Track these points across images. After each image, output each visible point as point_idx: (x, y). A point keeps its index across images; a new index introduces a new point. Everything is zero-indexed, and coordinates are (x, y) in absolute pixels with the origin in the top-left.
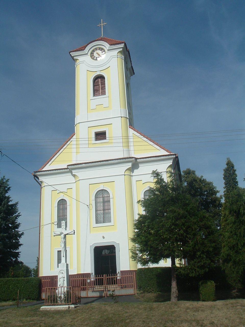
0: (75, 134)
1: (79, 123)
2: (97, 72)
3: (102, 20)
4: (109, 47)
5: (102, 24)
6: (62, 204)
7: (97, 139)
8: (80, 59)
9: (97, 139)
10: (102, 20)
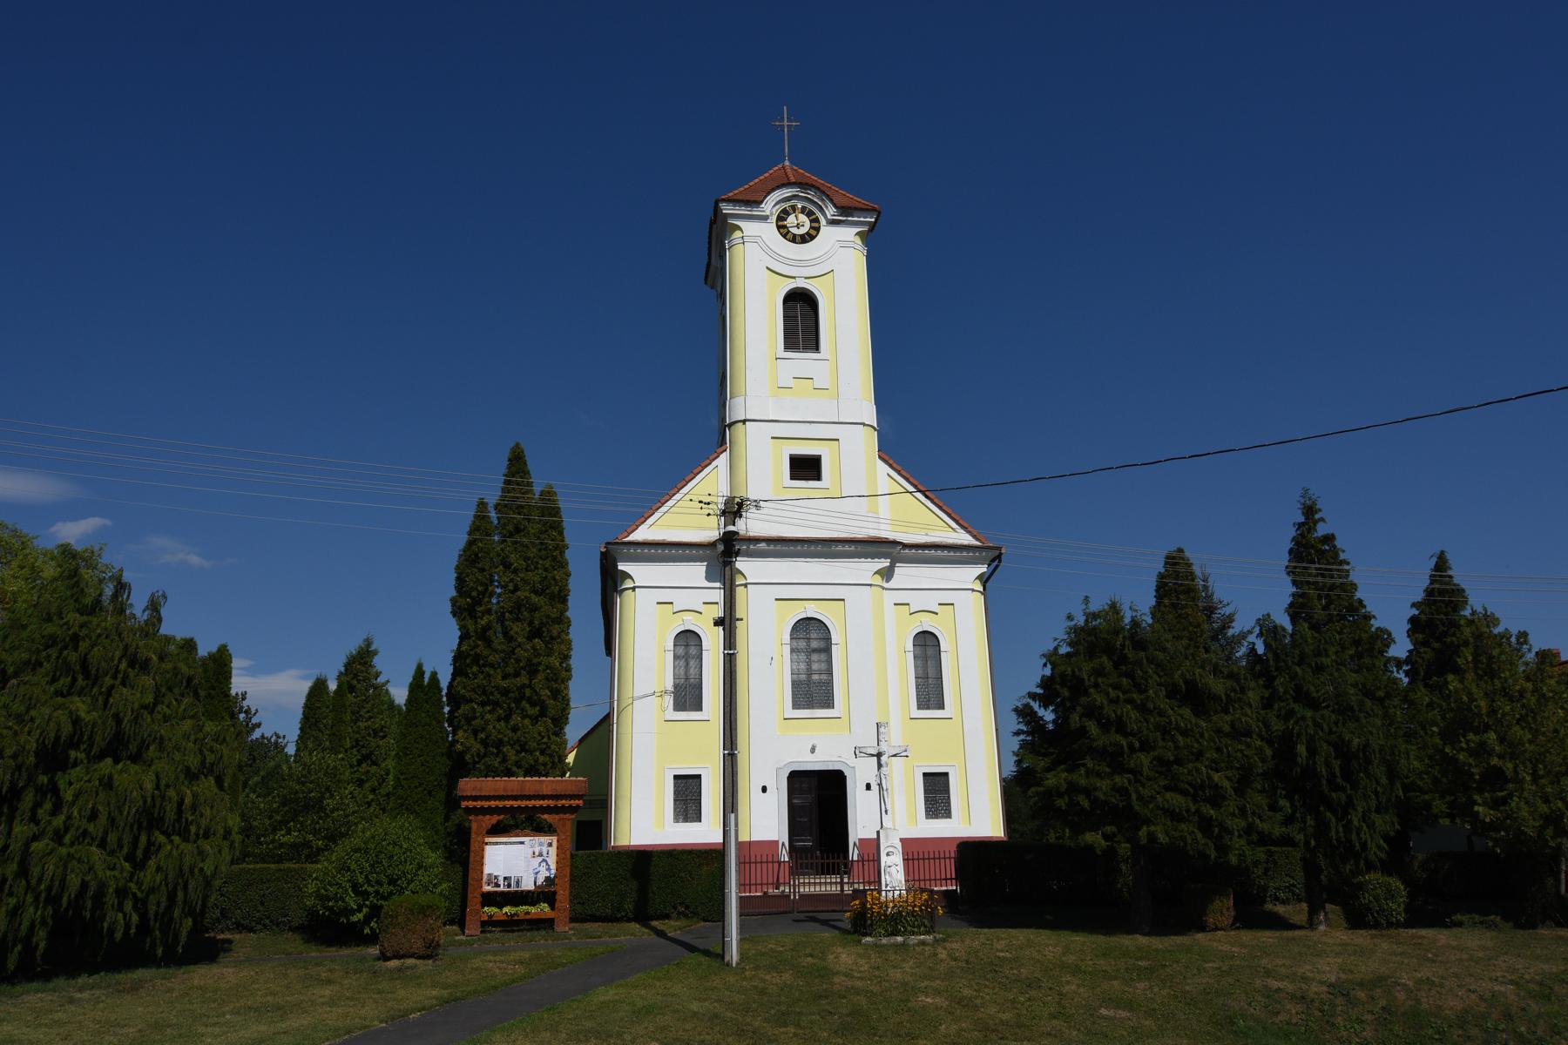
0: (726, 450)
1: (744, 422)
2: (794, 278)
3: (785, 108)
4: (832, 213)
5: (786, 123)
6: (930, 693)
7: (795, 475)
8: (749, 228)
9: (795, 475)
10: (785, 108)
